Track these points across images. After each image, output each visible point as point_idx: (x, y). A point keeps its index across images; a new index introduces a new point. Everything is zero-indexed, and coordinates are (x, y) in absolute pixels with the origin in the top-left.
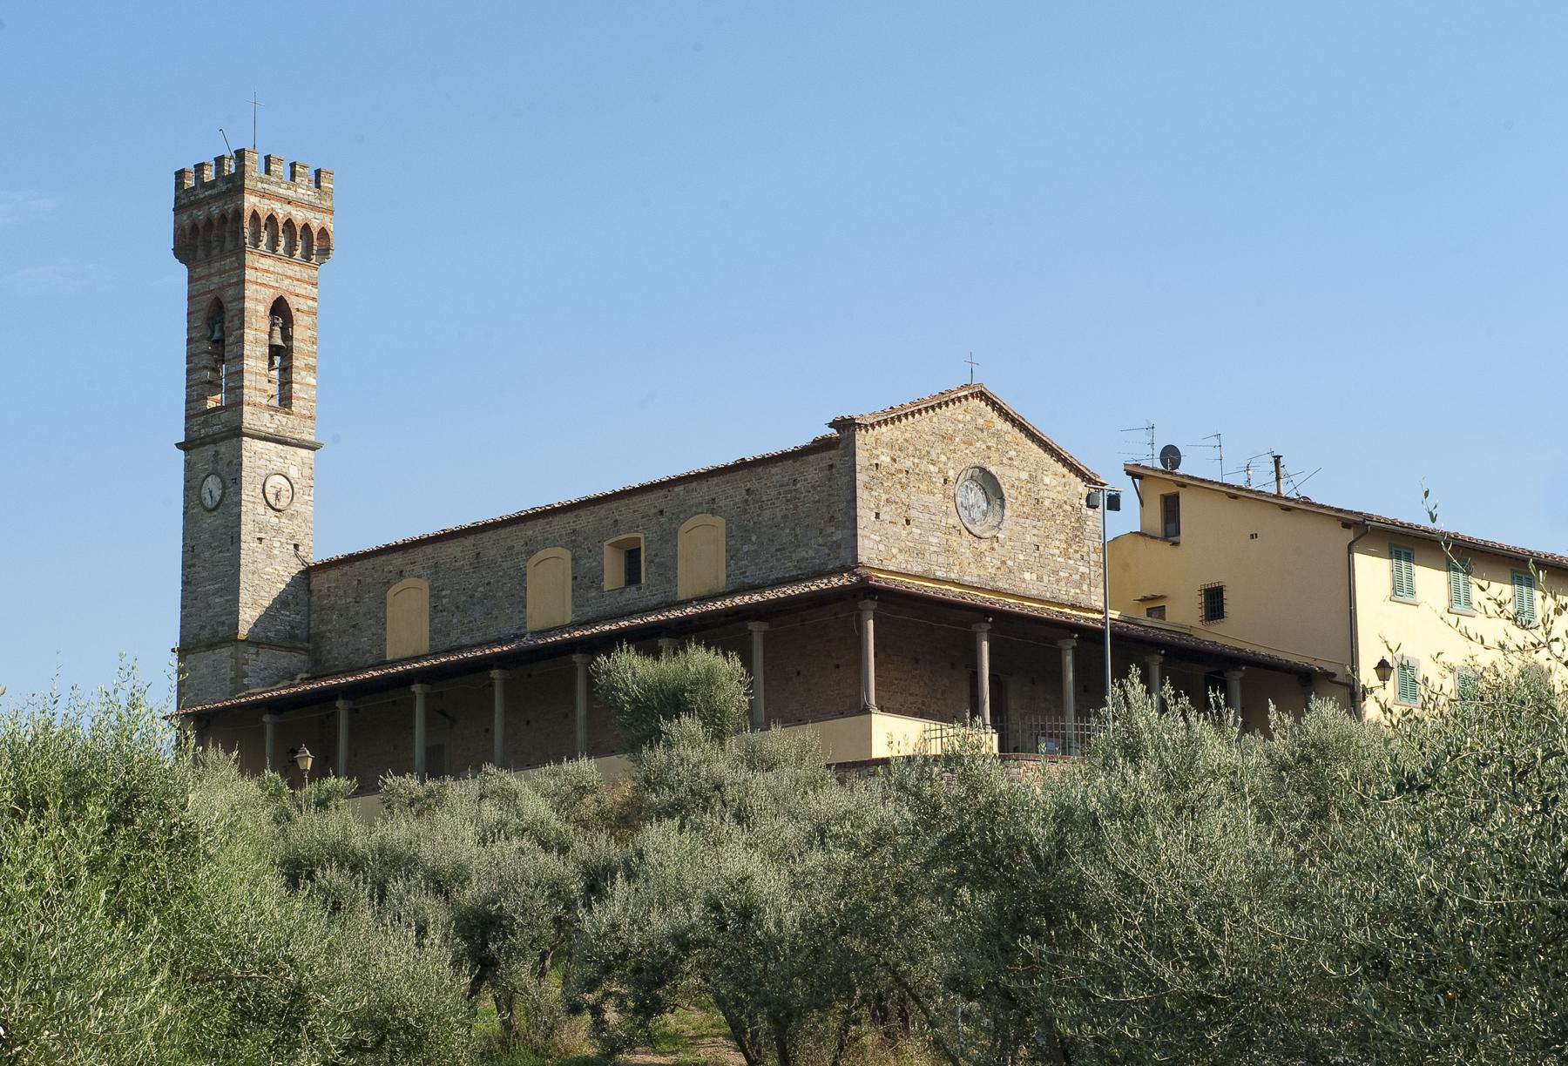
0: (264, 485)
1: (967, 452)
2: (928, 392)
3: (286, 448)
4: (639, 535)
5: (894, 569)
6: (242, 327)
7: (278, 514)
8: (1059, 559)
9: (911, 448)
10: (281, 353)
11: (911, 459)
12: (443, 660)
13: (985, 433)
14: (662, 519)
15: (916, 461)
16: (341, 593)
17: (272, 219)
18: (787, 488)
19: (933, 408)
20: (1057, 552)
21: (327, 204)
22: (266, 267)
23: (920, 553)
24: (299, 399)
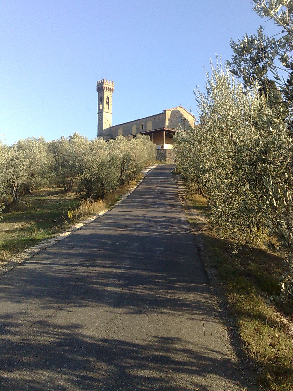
10: (108, 103)
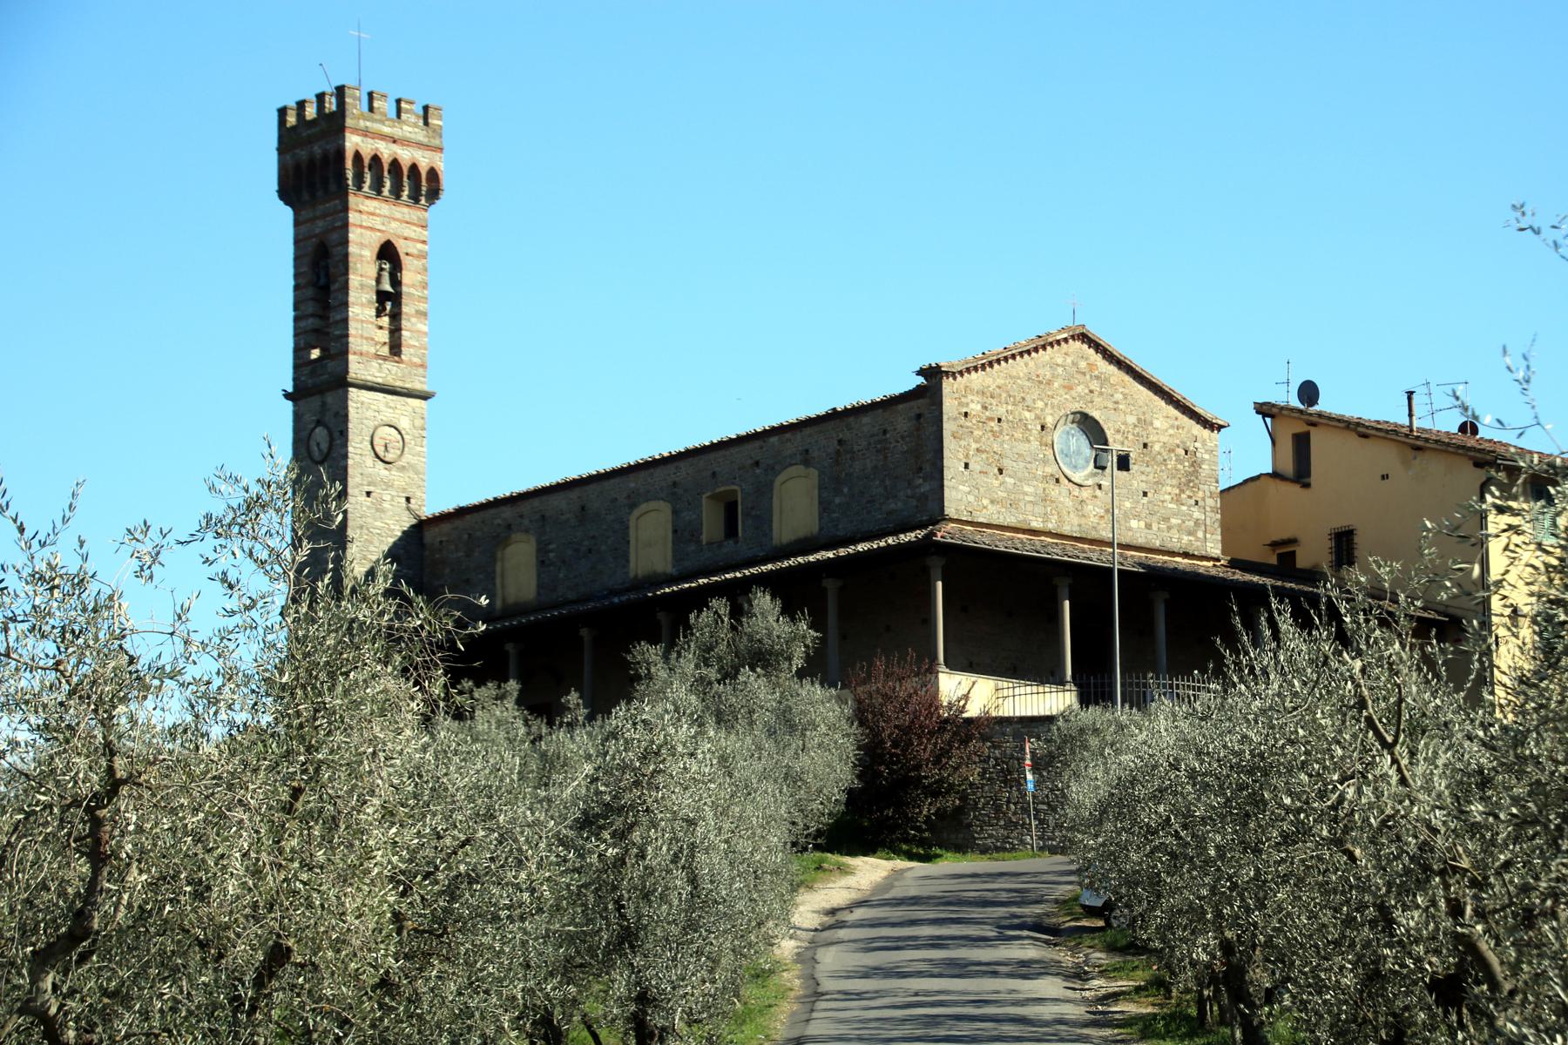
0: (372, 437)
1: (1067, 397)
2: (1023, 338)
3: (395, 398)
4: (735, 487)
5: (985, 521)
6: (346, 273)
7: (387, 466)
8: (1171, 506)
9: (1004, 395)
10: (389, 301)
11: (1005, 406)
12: (667, 590)
13: (1088, 377)
14: (758, 471)
15: (1010, 408)
16: (452, 547)
17: (376, 159)
18: (876, 438)
19: (1029, 352)
20: (1168, 497)
21: (436, 142)
22: (372, 210)
23: (1013, 505)
24: (410, 346)
